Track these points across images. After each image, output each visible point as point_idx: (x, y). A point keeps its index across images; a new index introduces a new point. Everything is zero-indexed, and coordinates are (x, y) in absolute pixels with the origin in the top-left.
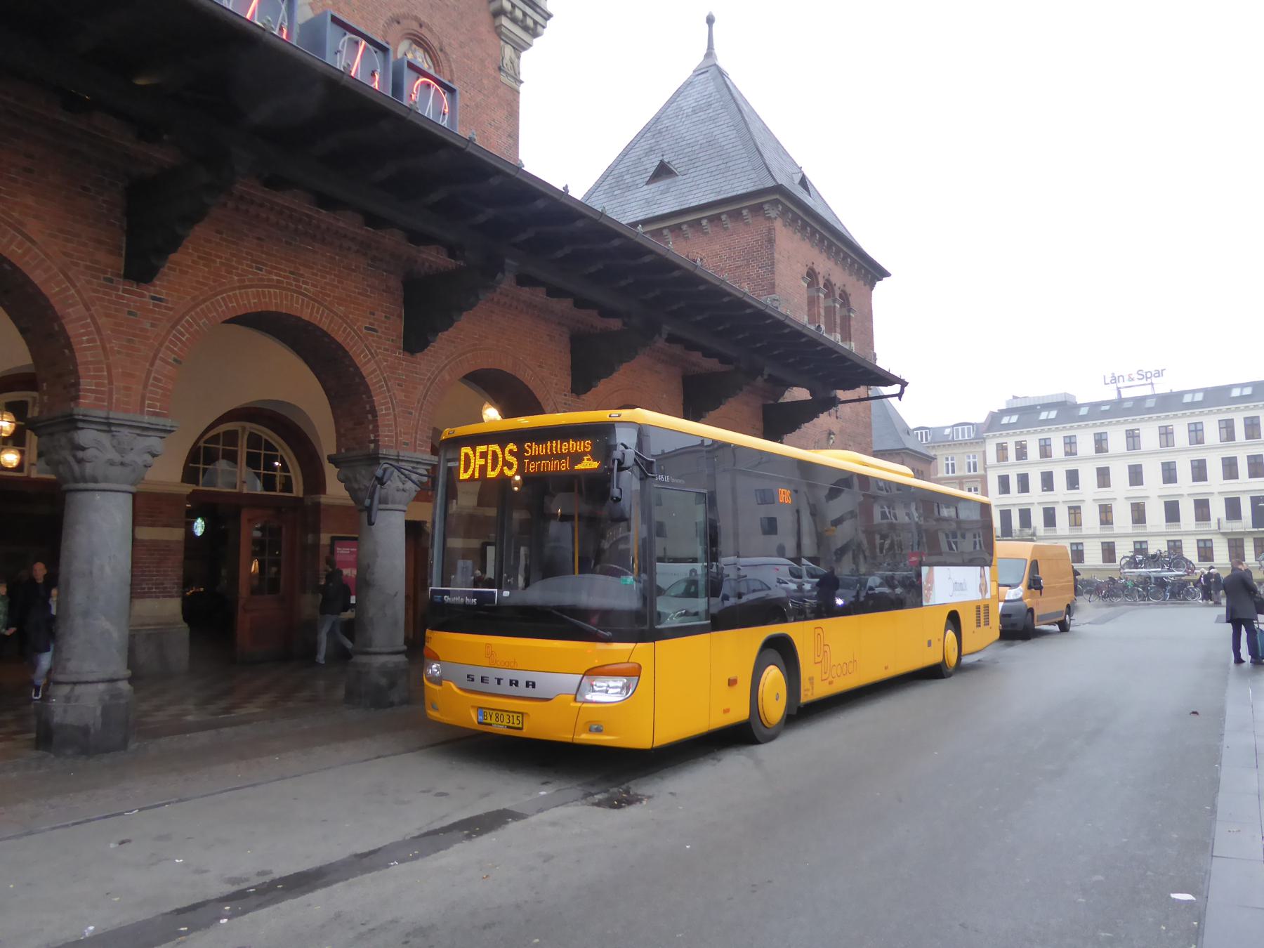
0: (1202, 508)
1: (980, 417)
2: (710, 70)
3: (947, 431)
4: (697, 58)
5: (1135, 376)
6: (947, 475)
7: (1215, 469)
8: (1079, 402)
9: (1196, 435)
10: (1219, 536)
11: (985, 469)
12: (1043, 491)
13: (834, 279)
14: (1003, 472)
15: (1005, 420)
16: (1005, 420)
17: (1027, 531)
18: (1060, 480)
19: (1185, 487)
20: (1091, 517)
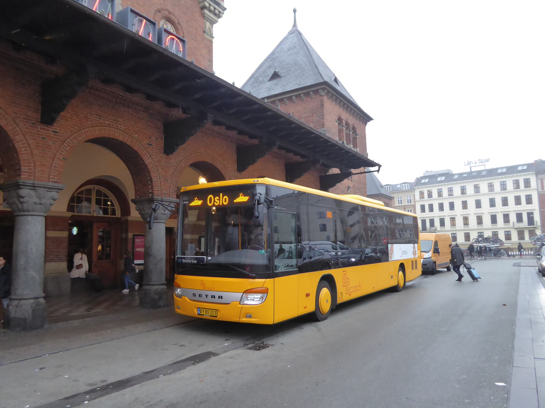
0: (506, 218)
1: (412, 180)
2: (295, 32)
3: (399, 186)
4: (290, 27)
5: (478, 162)
6: (399, 205)
7: (511, 201)
8: (454, 173)
9: (504, 187)
10: (514, 229)
11: (415, 202)
12: (440, 211)
13: (349, 122)
14: (422, 203)
15: (423, 181)
16: (423, 181)
17: (433, 228)
18: (446, 206)
19: (499, 209)
20: (459, 222)
